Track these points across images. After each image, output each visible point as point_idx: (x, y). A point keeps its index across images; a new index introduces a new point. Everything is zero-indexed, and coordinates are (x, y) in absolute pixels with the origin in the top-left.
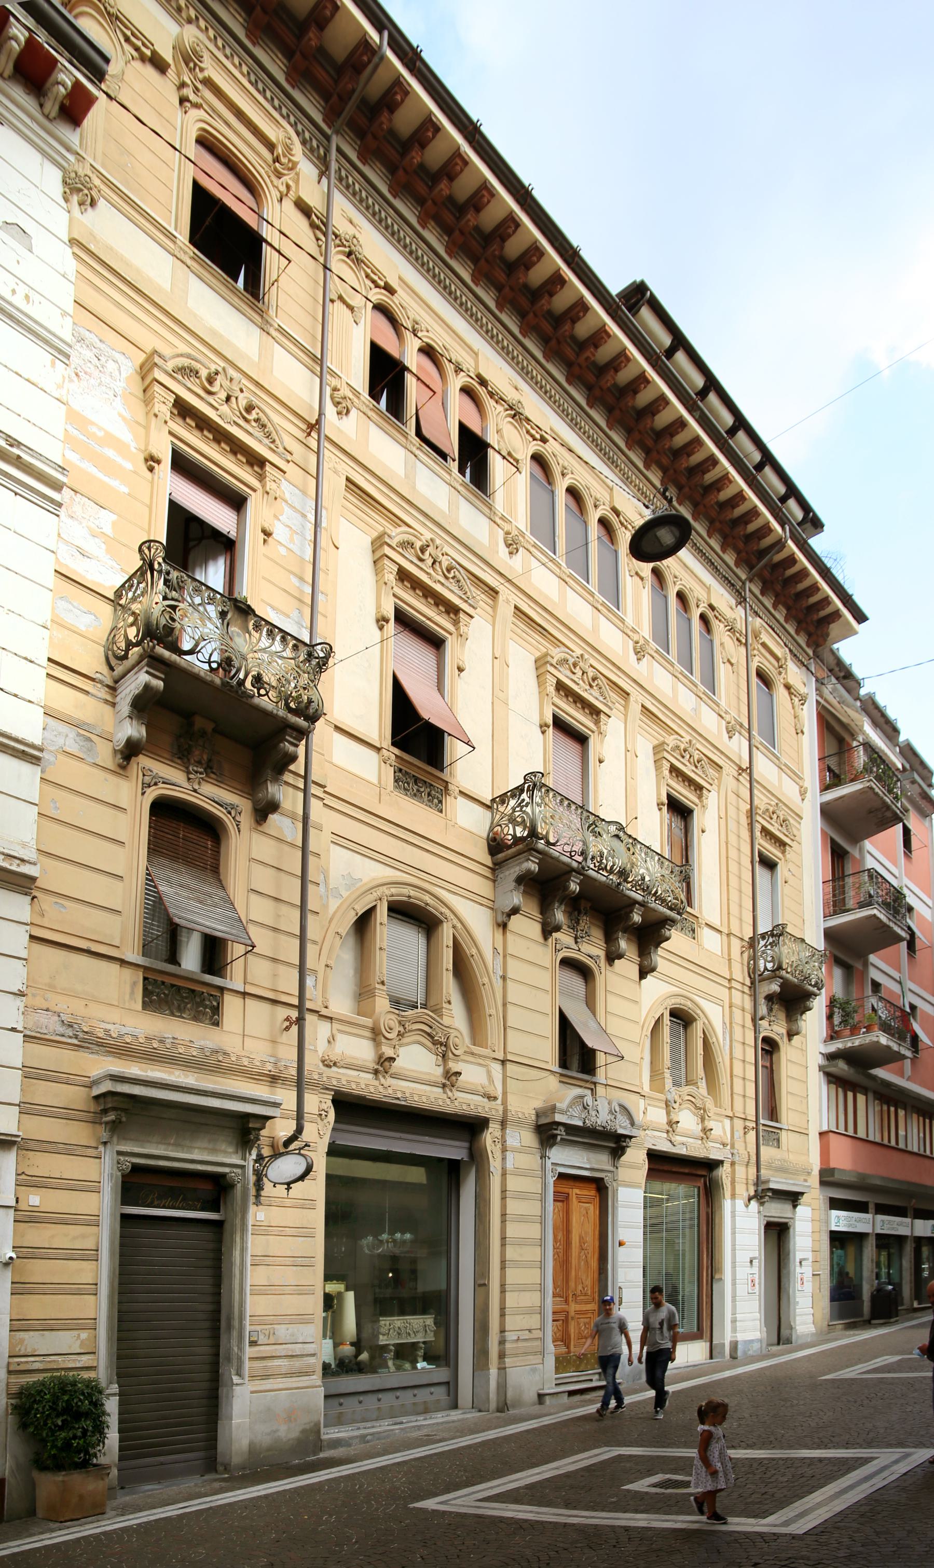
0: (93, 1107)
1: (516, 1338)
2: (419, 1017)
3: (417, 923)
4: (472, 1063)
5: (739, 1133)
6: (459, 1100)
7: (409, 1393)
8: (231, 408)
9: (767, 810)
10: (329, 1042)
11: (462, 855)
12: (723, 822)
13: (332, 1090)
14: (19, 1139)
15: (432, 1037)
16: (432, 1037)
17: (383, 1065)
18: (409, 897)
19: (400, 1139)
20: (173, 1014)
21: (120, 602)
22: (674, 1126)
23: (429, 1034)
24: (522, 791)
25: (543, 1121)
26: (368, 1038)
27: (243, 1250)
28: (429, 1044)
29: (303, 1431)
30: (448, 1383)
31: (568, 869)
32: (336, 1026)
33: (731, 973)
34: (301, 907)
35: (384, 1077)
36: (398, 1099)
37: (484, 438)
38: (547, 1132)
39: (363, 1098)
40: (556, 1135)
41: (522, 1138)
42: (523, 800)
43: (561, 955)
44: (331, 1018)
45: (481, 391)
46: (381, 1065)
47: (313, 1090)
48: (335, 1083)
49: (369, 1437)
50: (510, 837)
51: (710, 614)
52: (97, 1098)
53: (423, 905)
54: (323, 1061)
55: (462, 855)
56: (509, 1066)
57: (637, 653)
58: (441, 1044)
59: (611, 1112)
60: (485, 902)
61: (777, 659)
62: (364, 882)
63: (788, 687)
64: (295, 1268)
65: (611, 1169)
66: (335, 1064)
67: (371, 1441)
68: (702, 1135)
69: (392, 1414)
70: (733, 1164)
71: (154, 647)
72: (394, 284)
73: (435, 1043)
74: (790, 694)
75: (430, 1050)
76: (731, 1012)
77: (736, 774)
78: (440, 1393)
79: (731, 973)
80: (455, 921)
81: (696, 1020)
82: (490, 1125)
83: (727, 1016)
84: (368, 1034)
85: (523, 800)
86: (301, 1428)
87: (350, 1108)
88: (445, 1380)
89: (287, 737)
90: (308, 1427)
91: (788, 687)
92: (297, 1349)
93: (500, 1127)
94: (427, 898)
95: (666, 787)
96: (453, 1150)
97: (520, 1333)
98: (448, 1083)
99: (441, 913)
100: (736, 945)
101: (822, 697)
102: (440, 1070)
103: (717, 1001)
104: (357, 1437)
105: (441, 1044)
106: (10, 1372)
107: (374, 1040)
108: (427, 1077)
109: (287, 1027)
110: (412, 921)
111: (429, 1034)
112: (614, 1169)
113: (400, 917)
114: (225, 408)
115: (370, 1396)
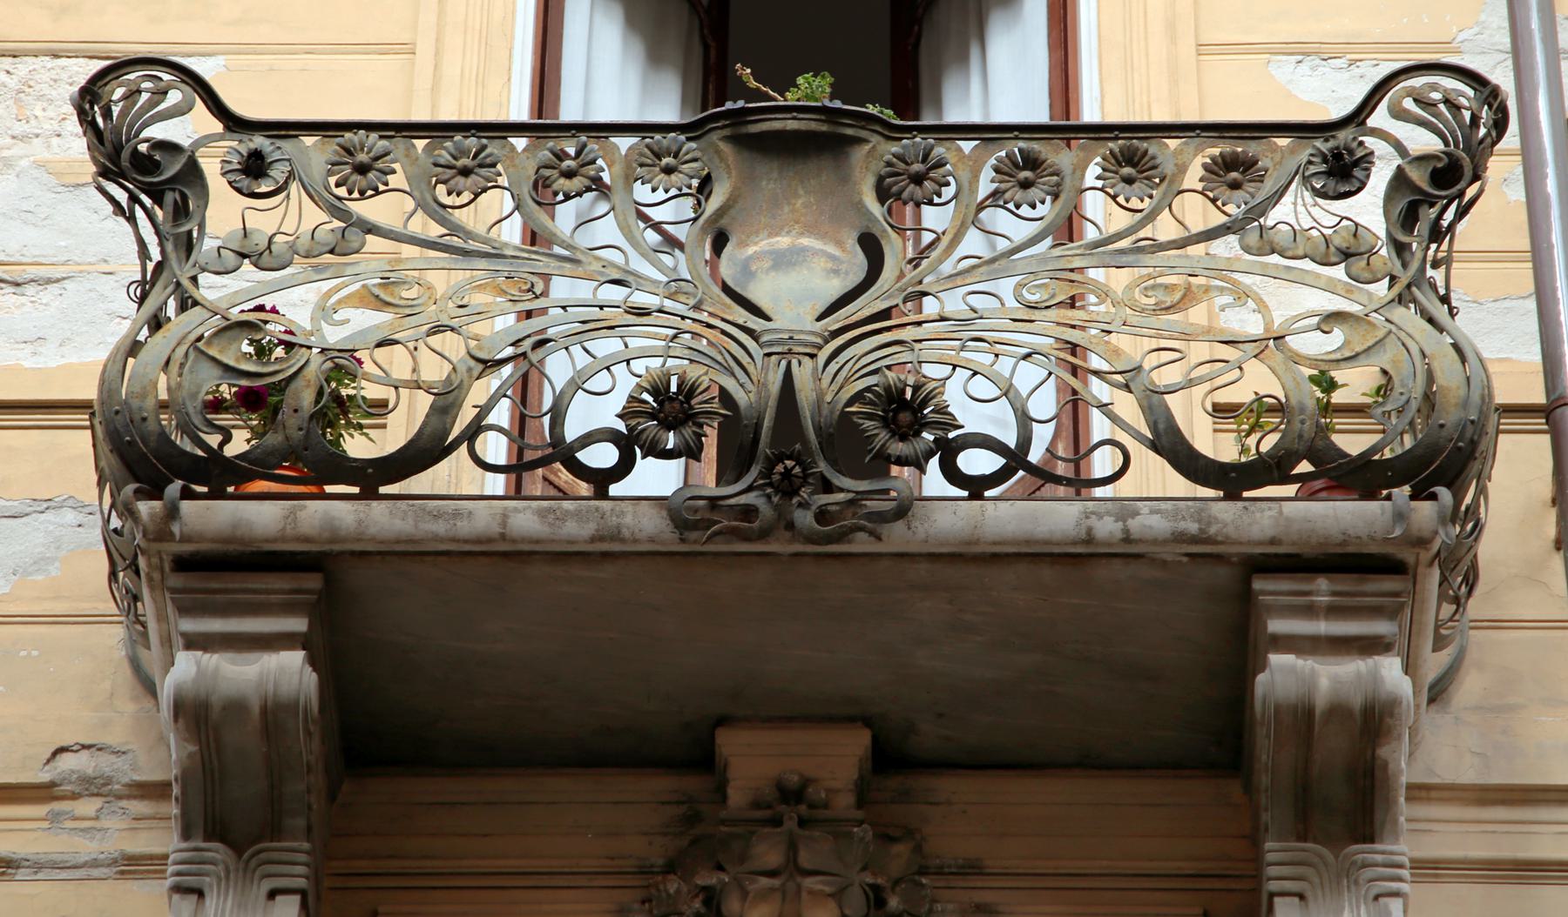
71: (172, 513)
89: (1277, 626)
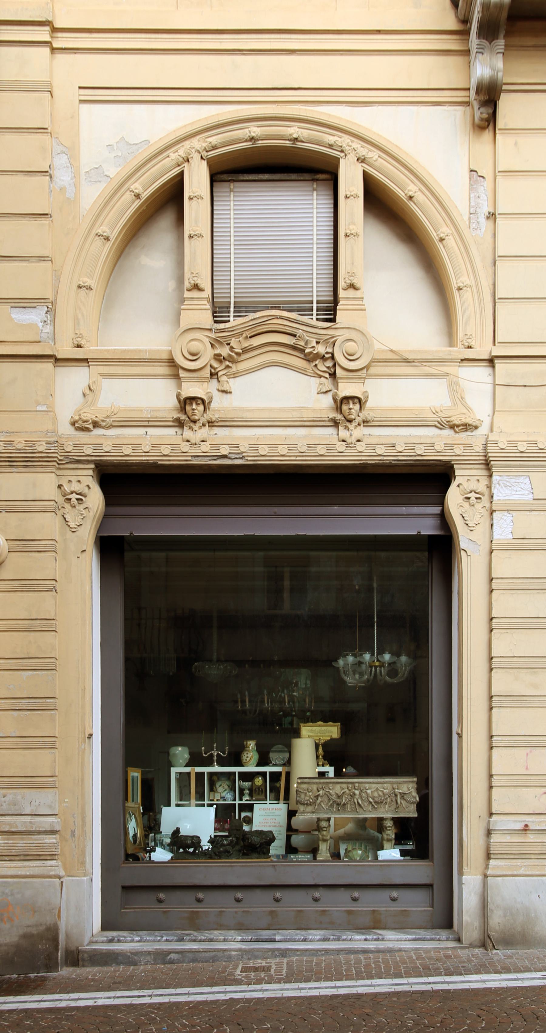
1: (520, 826)
2: (260, 324)
3: (307, 176)
4: (407, 376)
6: (366, 440)
7: (344, 895)
10: (84, 395)
11: (379, 32)
13: (89, 462)
15: (302, 351)
16: (302, 351)
17: (345, 409)
18: (252, 139)
19: (276, 515)
23: (294, 348)
26: (164, 376)
28: (300, 363)
29: (25, 936)
30: (430, 886)
32: (96, 369)
36: (225, 457)
39: (155, 465)
44: (86, 360)
47: (42, 467)
48: (89, 451)
49: (172, 956)
53: (288, 143)
54: (73, 424)
55: (379, 32)
56: (499, 364)
58: (323, 358)
62: (151, 143)
64: (15, 713)
66: (96, 424)
67: (178, 961)
68: (333, 415)
69: (325, 922)
73: (311, 358)
75: (303, 372)
78: (417, 904)
82: (457, 473)
84: (163, 370)
86: (21, 932)
87: (122, 482)
88: (427, 881)
90: (34, 931)
92: (20, 823)
93: (485, 473)
94: (294, 130)
96: (408, 521)
97: (528, 819)
99: (331, 146)
102: (327, 401)
104: (149, 953)
105: (323, 358)
108: (296, 415)
110: (294, 176)
111: (294, 348)
113: (266, 176)
115: (258, 893)
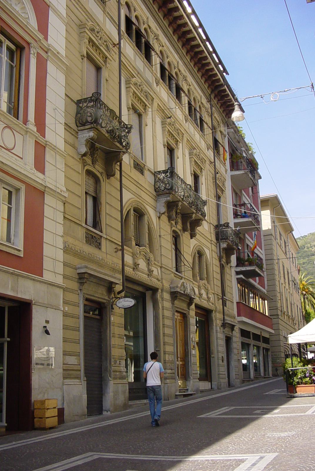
0: (77, 277)
5: (216, 299)
8: (101, 41)
9: (170, 123)
12: (206, 181)
14: (65, 287)
20: (90, 244)
21: (80, 105)
22: (137, 266)
24: (167, 172)
25: (173, 290)
27: (110, 331)
31: (192, 212)
33: (211, 238)
34: (121, 211)
35: (136, 270)
37: (164, 65)
38: (174, 295)
40: (177, 296)
41: (167, 296)
42: (168, 175)
43: (86, 168)
45: (149, 30)
46: (135, 266)
50: (163, 187)
51: (201, 106)
52: (78, 274)
56: (163, 269)
57: (157, 83)
59: (190, 290)
60: (153, 207)
61: (218, 122)
63: (221, 132)
65: (187, 310)
70: (162, 290)
72: (164, 45)
73: (205, 288)
74: (221, 134)
76: (212, 253)
77: (209, 163)
79: (211, 238)
80: (149, 215)
81: (203, 255)
83: (211, 254)
85: (168, 175)
91: (221, 132)
95: (131, 101)
98: (150, 274)
100: (212, 227)
101: (229, 136)
103: (208, 249)
106: (64, 370)
107: (133, 257)
109: (116, 251)
112: (188, 310)
114: (100, 41)
